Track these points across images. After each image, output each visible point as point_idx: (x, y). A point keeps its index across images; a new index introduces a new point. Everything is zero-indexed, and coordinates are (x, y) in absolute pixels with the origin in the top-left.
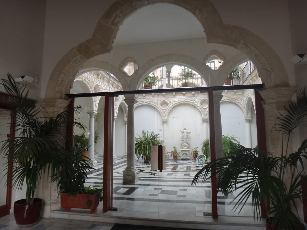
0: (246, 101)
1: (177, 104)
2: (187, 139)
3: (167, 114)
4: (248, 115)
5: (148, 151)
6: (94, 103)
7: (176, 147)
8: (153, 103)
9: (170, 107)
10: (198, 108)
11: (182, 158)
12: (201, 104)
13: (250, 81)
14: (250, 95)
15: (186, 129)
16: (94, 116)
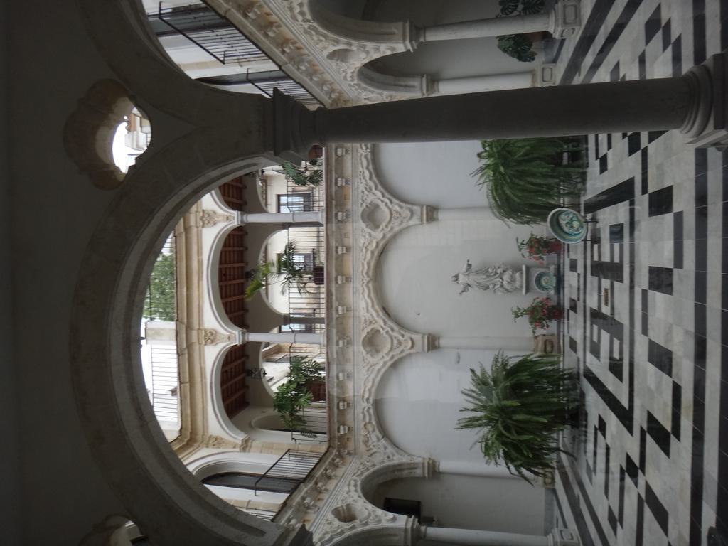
0: (372, 92)
1: (375, 303)
2: (487, 271)
3: (407, 335)
4: (414, 87)
5: (535, 418)
6: (385, 524)
7: (515, 309)
8: (371, 379)
9: (382, 324)
10: (389, 236)
11: (552, 292)
12: (376, 226)
13: (316, 79)
14: (349, 72)
15: (457, 277)
16: (423, 528)
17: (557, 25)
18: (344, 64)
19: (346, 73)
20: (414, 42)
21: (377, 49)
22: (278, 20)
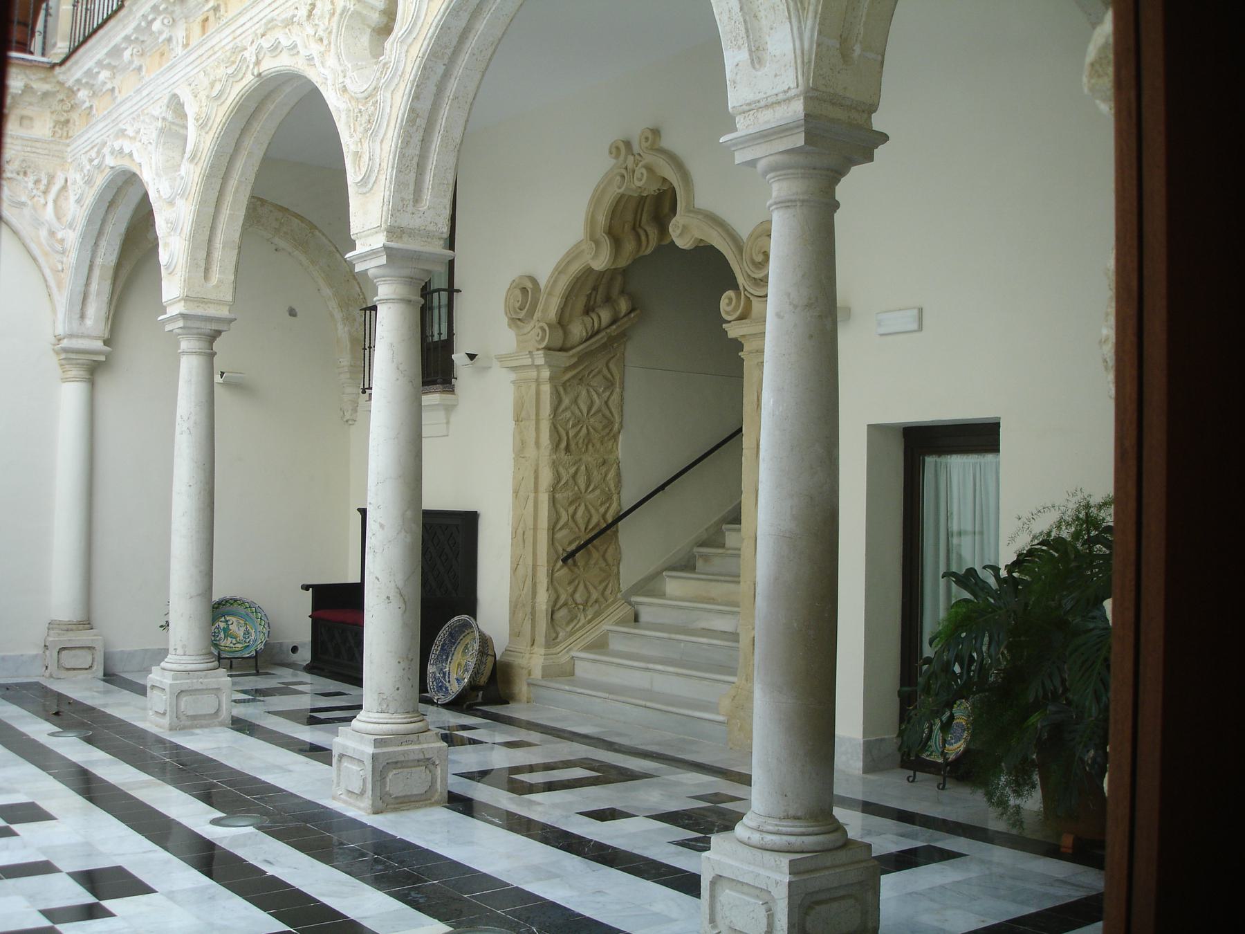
17: (178, 674)
18: (154, 135)
19: (132, 139)
20: (181, 324)
21: (173, 226)
22: (230, 15)
